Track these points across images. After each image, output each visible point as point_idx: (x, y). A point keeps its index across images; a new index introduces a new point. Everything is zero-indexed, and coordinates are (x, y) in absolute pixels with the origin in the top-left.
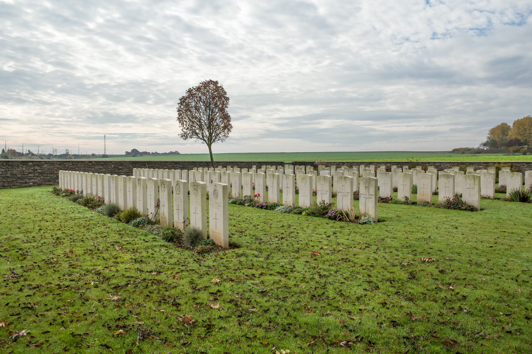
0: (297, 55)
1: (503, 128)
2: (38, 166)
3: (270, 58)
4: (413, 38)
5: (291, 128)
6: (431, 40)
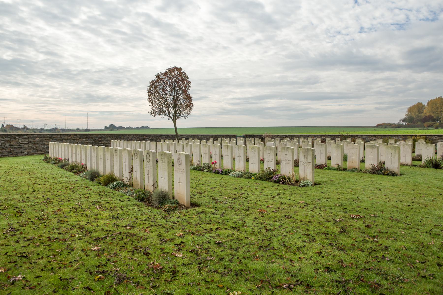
0: (248, 45)
1: (419, 107)
2: (32, 138)
3: (225, 48)
4: (343, 32)
6: (359, 34)
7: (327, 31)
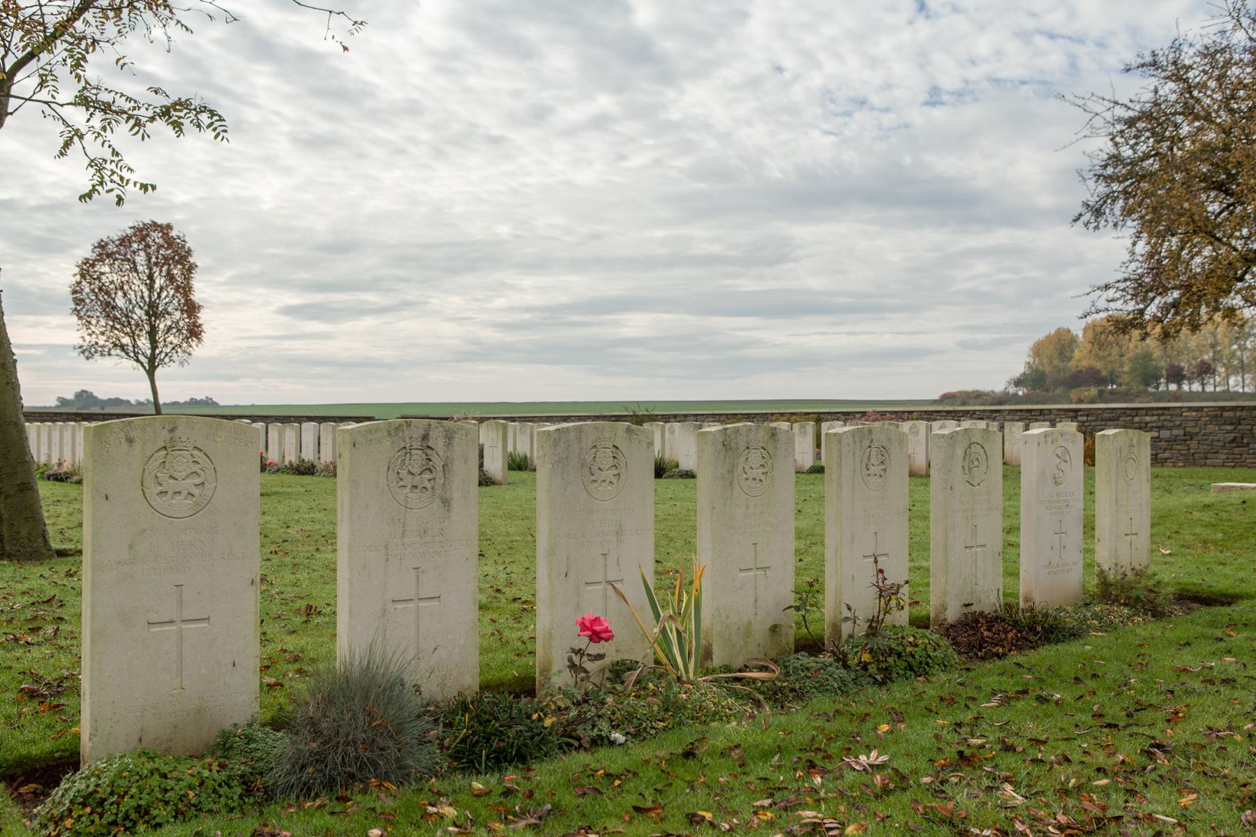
0: (569, 132)
1: (1061, 343)
3: (496, 141)
4: (876, 100)
5: (998, 336)
6: (926, 108)
7: (827, 95)
